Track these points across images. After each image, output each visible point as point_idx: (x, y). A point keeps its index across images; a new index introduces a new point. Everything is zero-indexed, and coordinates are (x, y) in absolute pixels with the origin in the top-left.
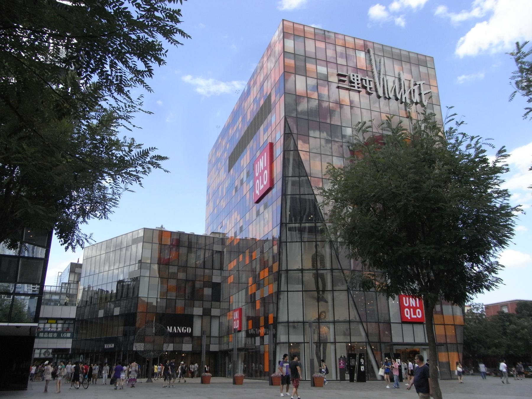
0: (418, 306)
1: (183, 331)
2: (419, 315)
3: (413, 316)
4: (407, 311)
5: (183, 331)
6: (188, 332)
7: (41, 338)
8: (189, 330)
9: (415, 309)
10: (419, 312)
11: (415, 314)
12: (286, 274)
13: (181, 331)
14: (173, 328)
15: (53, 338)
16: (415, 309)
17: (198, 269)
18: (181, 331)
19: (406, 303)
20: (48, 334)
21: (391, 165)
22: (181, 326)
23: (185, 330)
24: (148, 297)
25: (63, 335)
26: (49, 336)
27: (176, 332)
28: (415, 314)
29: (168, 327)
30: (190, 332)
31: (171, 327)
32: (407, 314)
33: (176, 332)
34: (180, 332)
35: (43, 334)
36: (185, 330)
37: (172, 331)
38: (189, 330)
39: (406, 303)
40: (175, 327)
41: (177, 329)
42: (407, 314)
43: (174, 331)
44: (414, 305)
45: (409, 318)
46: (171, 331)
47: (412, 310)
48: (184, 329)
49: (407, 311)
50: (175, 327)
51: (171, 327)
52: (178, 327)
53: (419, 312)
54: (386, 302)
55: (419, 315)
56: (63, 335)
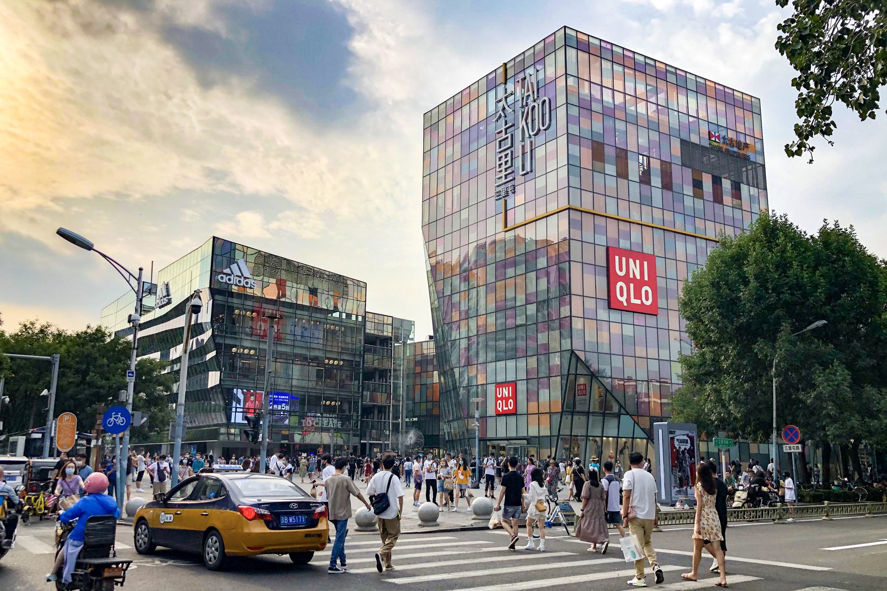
0: (646, 278)
2: (647, 299)
3: (505, 409)
9: (507, 399)
10: (647, 292)
11: (638, 296)
16: (639, 284)
19: (621, 270)
28: (638, 296)
32: (622, 295)
39: (621, 270)
42: (622, 295)
47: (632, 285)
49: (621, 288)
53: (647, 292)
55: (647, 299)
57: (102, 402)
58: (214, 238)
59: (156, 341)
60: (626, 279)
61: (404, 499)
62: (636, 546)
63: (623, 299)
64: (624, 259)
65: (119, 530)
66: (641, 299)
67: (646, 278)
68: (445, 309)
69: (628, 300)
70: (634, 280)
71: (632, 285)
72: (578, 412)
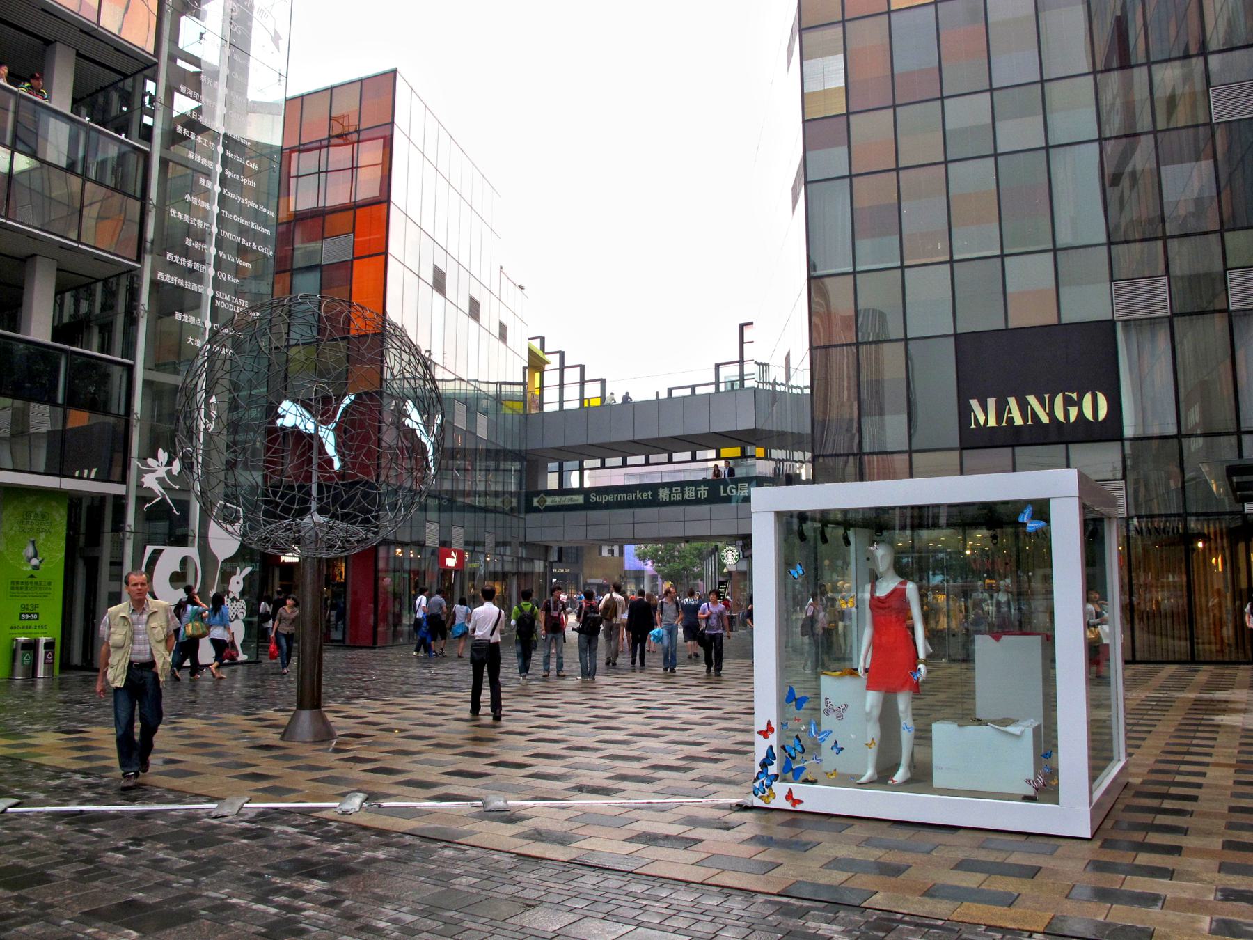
1: (1060, 415)
5: (1060, 415)
6: (1089, 415)
7: (537, 510)
8: (1095, 407)
13: (1051, 414)
14: (1001, 409)
15: (697, 501)
17: (1212, 229)
18: (1051, 414)
20: (682, 491)
22: (1045, 390)
23: (1073, 412)
24: (854, 273)
25: (725, 491)
26: (686, 497)
27: (1018, 421)
29: (974, 403)
30: (1102, 414)
31: (991, 402)
33: (1018, 421)
34: (1045, 419)
35: (667, 490)
36: (1073, 412)
37: (999, 418)
38: (1095, 407)
40: (1012, 401)
41: (1023, 406)
43: (1011, 420)
46: (992, 422)
48: (1068, 402)
50: (1012, 401)
51: (991, 402)
52: (1032, 400)
54: (961, 832)
56: (725, 491)
72: (897, 10)
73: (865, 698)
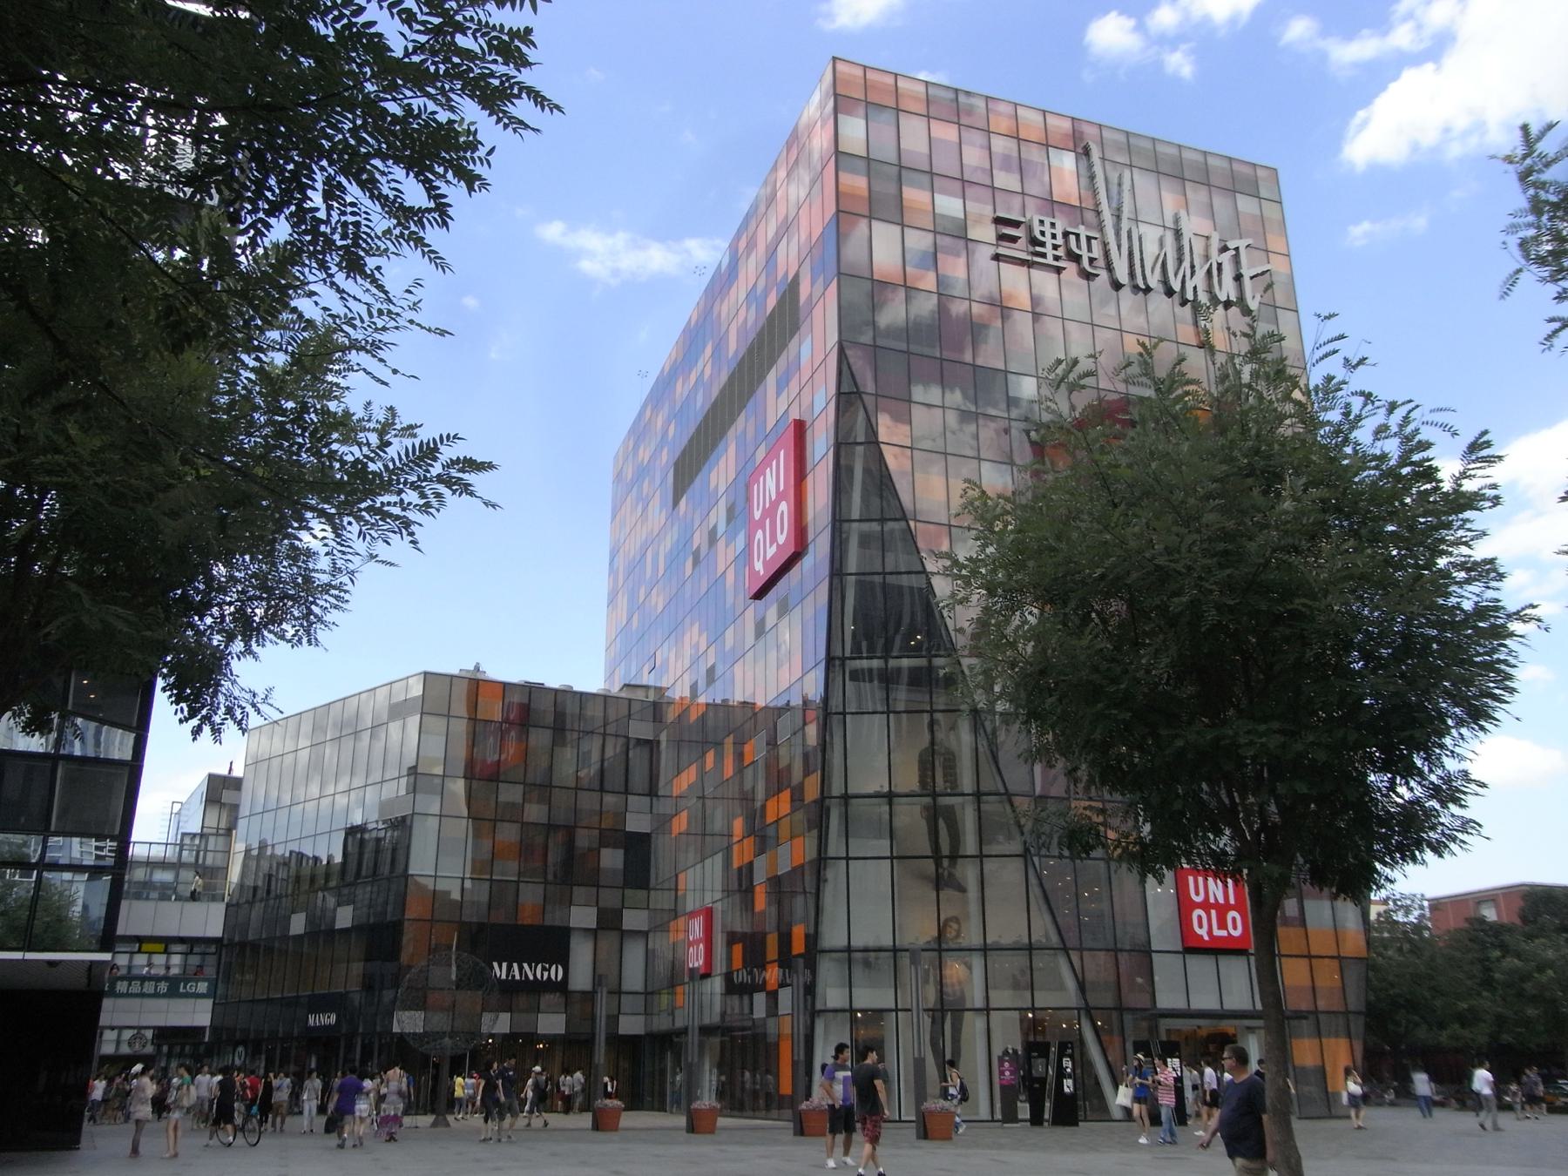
0: (1232, 901)
1: (539, 976)
2: (1235, 928)
3: (1217, 932)
4: (1200, 918)
5: (539, 976)
6: (553, 977)
7: (122, 995)
8: (557, 973)
9: (1222, 910)
10: (1234, 919)
11: (1222, 925)
12: (843, 809)
13: (535, 975)
14: (509, 968)
15: (156, 995)
16: (1222, 910)
18: (535, 975)
19: (1197, 893)
20: (142, 985)
21: (1152, 486)
22: (533, 960)
23: (546, 974)
24: (436, 877)
25: (185, 987)
26: (145, 990)
27: (518, 977)
28: (1222, 925)
29: (495, 965)
30: (560, 978)
31: (504, 965)
32: (1201, 926)
33: (518, 977)
34: (531, 978)
35: (125, 983)
36: (546, 974)
37: (507, 976)
38: (557, 973)
39: (1197, 893)
40: (515, 965)
41: (521, 969)
42: (1201, 926)
43: (514, 976)
44: (1221, 900)
45: (1206, 938)
46: (504, 977)
47: (1213, 913)
48: (544, 969)
49: (1200, 918)
50: (515, 965)
51: (504, 965)
52: (525, 965)
53: (1234, 919)
55: (1235, 928)
56: (185, 987)
57: (1366, 1080)
58: (834, 59)
59: (223, 709)
60: (1205, 905)
61: (129, 1150)
62: (800, 428)
63: (1203, 932)
64: (1200, 879)
65: (420, 1015)
66: (1227, 929)
67: (1232, 901)
68: (680, 662)
69: (1210, 932)
70: (1216, 906)
71: (1213, 913)
72: (1117, 959)
73: (725, 1129)
